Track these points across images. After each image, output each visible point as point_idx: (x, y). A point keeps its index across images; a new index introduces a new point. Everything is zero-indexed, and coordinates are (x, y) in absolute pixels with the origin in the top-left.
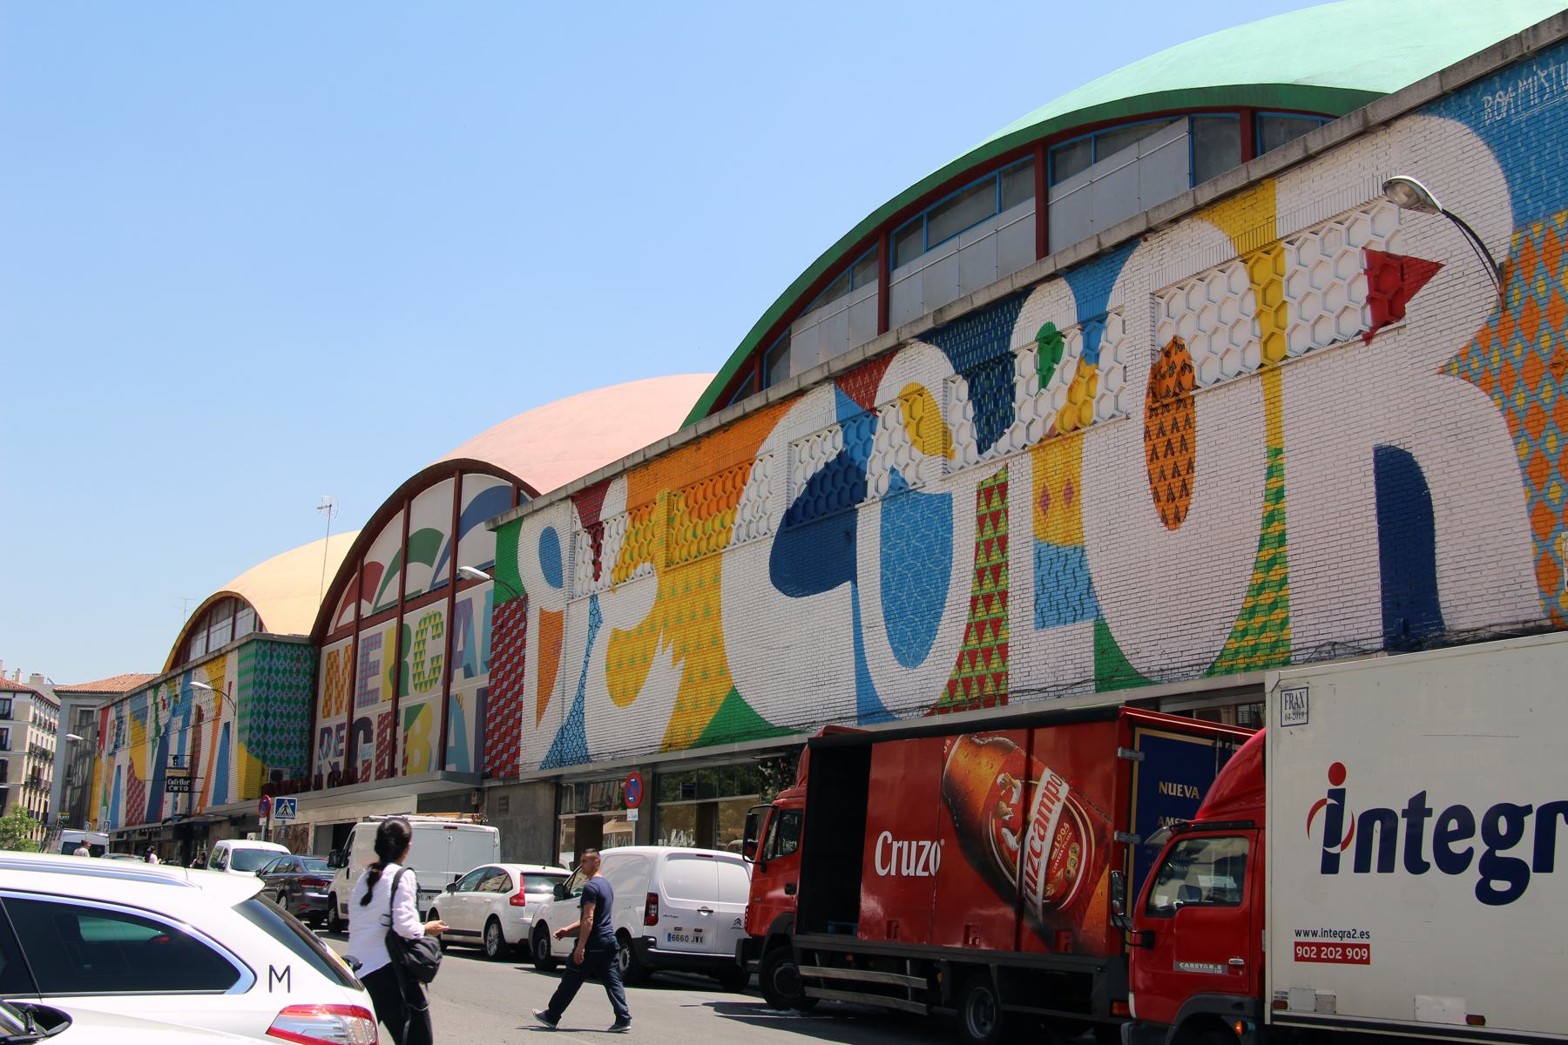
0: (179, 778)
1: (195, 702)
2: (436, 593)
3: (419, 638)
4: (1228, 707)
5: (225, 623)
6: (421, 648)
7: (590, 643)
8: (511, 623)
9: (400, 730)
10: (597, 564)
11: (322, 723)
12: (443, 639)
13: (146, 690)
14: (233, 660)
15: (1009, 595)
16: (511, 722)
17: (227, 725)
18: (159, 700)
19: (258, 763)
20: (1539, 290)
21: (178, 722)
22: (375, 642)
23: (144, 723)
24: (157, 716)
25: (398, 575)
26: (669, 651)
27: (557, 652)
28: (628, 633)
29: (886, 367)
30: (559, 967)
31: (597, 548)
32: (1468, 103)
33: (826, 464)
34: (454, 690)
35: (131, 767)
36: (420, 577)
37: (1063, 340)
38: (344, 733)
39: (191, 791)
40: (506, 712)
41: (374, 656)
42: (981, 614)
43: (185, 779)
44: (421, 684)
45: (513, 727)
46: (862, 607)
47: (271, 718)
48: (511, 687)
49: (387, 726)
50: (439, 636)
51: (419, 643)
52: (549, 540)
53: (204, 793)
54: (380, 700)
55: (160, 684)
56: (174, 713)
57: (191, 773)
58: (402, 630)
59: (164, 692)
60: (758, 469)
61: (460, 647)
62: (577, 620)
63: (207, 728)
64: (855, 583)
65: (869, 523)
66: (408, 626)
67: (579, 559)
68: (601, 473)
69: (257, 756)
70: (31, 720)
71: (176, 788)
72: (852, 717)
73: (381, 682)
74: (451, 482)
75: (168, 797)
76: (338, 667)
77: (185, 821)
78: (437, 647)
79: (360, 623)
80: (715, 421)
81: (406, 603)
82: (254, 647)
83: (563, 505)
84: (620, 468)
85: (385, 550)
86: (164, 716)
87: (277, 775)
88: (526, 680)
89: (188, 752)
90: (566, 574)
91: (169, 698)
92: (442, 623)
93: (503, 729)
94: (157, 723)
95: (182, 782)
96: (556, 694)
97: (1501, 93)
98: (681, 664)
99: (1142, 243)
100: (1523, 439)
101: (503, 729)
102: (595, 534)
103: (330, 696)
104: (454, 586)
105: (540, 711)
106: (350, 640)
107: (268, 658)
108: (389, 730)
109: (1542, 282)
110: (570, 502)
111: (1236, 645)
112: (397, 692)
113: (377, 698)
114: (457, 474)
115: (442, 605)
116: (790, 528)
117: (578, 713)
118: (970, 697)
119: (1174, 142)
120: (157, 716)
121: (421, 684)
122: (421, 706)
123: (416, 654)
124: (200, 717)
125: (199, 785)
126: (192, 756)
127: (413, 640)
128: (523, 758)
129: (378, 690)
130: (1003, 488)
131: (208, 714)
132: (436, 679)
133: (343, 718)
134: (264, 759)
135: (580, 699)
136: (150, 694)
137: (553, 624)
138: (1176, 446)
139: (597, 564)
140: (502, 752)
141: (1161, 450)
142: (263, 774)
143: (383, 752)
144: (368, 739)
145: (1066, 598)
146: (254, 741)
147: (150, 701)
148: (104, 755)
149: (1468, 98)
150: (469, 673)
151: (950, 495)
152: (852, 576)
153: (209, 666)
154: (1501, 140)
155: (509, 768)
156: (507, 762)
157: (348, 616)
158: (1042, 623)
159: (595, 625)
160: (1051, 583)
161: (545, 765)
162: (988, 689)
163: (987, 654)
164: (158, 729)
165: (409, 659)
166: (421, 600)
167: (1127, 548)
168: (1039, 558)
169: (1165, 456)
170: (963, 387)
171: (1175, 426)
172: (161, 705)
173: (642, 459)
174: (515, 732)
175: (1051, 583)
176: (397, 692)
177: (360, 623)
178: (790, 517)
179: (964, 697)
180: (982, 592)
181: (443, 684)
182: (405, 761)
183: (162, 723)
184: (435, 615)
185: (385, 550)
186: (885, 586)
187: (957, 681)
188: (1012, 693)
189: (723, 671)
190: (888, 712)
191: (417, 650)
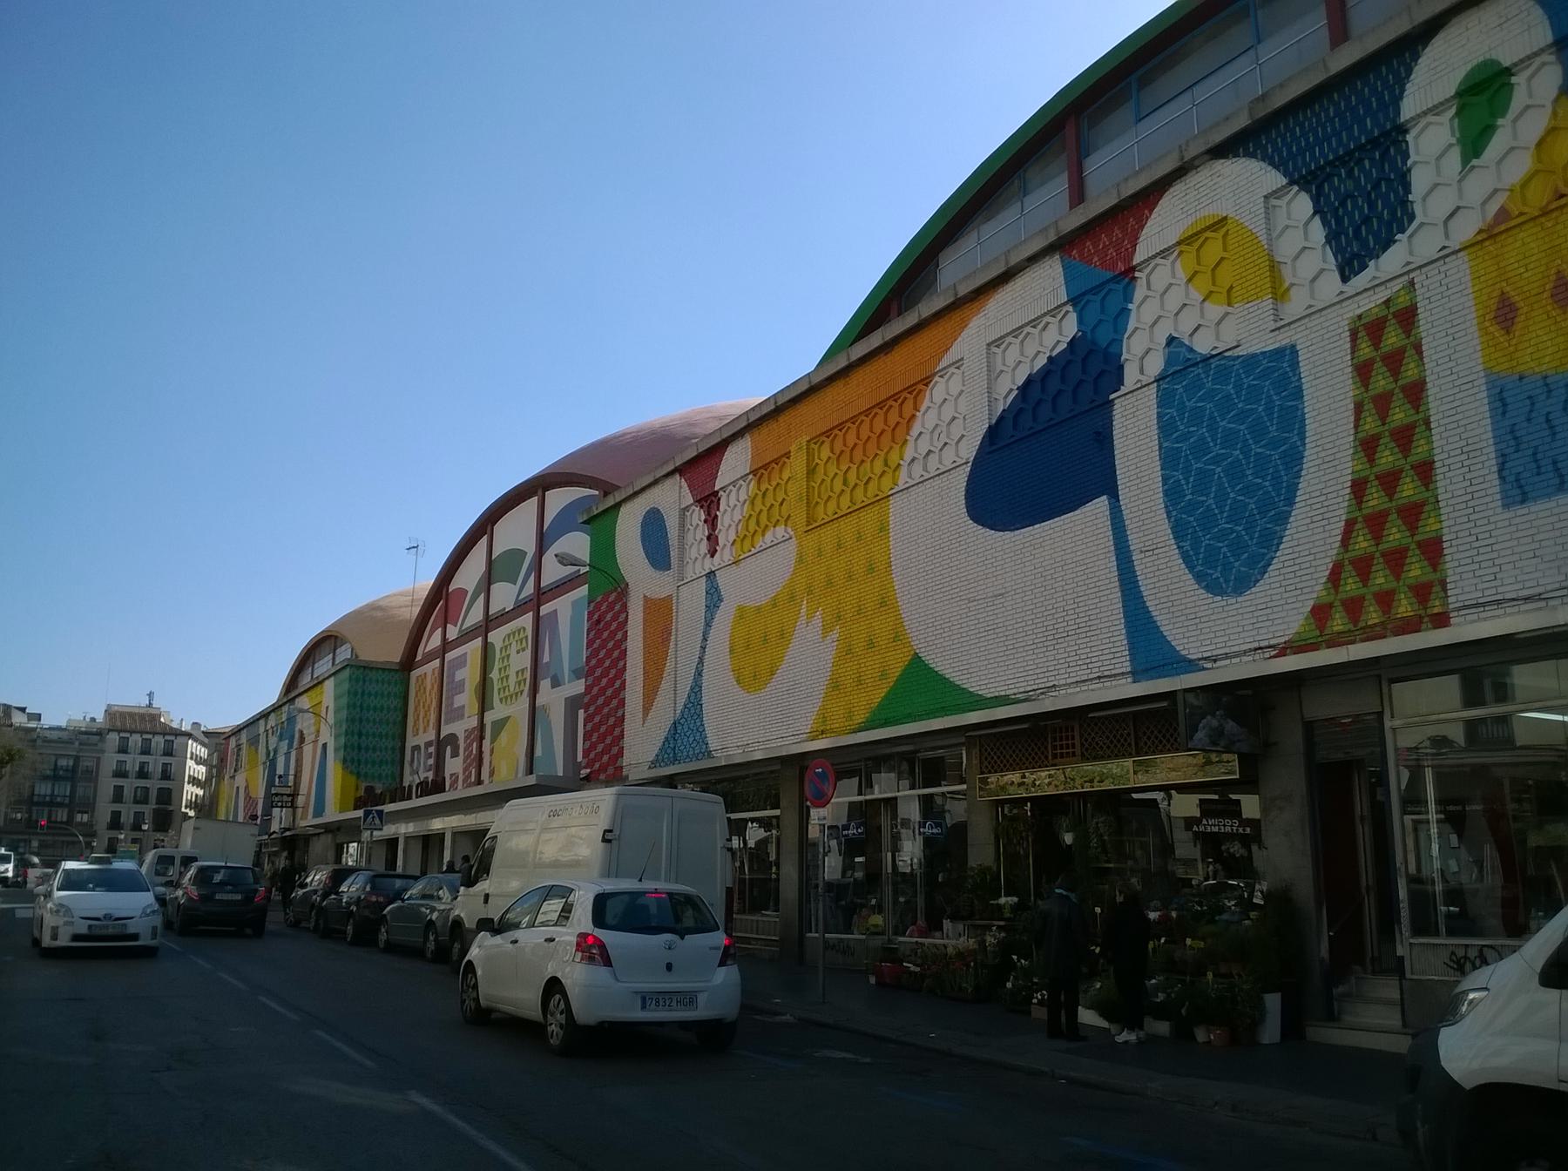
0: (282, 795)
1: (298, 727)
2: (520, 608)
3: (504, 654)
5: (326, 659)
6: (506, 663)
7: (708, 625)
8: (609, 617)
9: (486, 743)
10: (712, 539)
11: (411, 741)
12: (528, 652)
13: (258, 719)
14: (329, 685)
15: (1437, 465)
16: (612, 721)
17: (325, 746)
18: (269, 727)
19: (352, 779)
21: (284, 745)
22: (461, 662)
23: (257, 750)
24: (267, 741)
25: (482, 597)
26: (817, 621)
27: (666, 641)
28: (758, 609)
29: (1151, 211)
31: (712, 521)
33: (1050, 359)
34: (540, 701)
35: (247, 787)
36: (504, 596)
38: (432, 749)
39: (293, 806)
40: (606, 710)
41: (460, 675)
42: (1375, 499)
43: (288, 795)
44: (506, 698)
45: (614, 726)
46: (1131, 526)
47: (364, 738)
48: (611, 683)
49: (473, 741)
50: (523, 650)
51: (503, 658)
52: (653, 524)
53: (305, 807)
54: (466, 715)
55: (269, 713)
56: (281, 738)
57: (294, 790)
58: (487, 648)
59: (272, 721)
60: (938, 390)
61: (546, 658)
62: (692, 601)
63: (308, 749)
64: (1114, 495)
66: (493, 644)
67: (690, 537)
68: (718, 434)
69: (351, 772)
70: (189, 756)
71: (280, 804)
72: (1123, 674)
73: (466, 699)
74: (533, 502)
75: (276, 811)
76: (425, 689)
77: (288, 833)
78: (523, 660)
79: (446, 646)
80: (875, 340)
81: (490, 622)
82: (347, 672)
83: (669, 482)
84: (744, 424)
85: (470, 575)
86: (273, 740)
87: (369, 790)
88: (628, 675)
89: (292, 772)
90: (674, 554)
91: (277, 725)
92: (527, 637)
93: (603, 729)
94: (267, 748)
95: (285, 798)
96: (666, 686)
98: (835, 635)
101: (603, 729)
102: (709, 506)
103: (418, 715)
104: (539, 599)
105: (647, 709)
106: (437, 663)
107: (361, 683)
108: (475, 744)
110: (677, 476)
112: (484, 704)
113: (463, 715)
114: (540, 492)
115: (527, 620)
116: (994, 448)
117: (694, 704)
118: (1362, 624)
120: (267, 741)
121: (506, 698)
122: (509, 717)
123: (500, 669)
124: (302, 739)
125: (300, 800)
126: (295, 776)
127: (498, 656)
128: (626, 760)
129: (464, 706)
130: (1407, 317)
131: (309, 738)
132: (522, 692)
133: (431, 735)
134: (358, 775)
135: (696, 689)
136: (262, 722)
137: (660, 613)
139: (712, 539)
140: (602, 753)
142: (357, 789)
143: (470, 765)
144: (455, 754)
145: (1536, 461)
146: (349, 758)
147: (262, 729)
148: (226, 777)
150: (556, 683)
151: (1293, 346)
152: (1108, 485)
153: (309, 693)
155: (611, 770)
156: (608, 764)
157: (435, 641)
158: (1517, 491)
159: (714, 598)
161: (654, 764)
162: (1401, 610)
163: (1396, 560)
164: (268, 754)
165: (494, 675)
166: (505, 617)
167: (1085, 587)
168: (1502, 400)
170: (1303, 204)
172: (270, 732)
173: (773, 407)
174: (617, 731)
176: (484, 704)
177: (446, 646)
178: (993, 433)
179: (1351, 626)
180: (1375, 470)
181: (529, 695)
182: (492, 773)
183: (271, 748)
184: (519, 631)
185: (470, 575)
186: (1172, 494)
187: (1330, 606)
188: (1459, 609)
189: (898, 636)
190: (1191, 661)
191: (500, 686)
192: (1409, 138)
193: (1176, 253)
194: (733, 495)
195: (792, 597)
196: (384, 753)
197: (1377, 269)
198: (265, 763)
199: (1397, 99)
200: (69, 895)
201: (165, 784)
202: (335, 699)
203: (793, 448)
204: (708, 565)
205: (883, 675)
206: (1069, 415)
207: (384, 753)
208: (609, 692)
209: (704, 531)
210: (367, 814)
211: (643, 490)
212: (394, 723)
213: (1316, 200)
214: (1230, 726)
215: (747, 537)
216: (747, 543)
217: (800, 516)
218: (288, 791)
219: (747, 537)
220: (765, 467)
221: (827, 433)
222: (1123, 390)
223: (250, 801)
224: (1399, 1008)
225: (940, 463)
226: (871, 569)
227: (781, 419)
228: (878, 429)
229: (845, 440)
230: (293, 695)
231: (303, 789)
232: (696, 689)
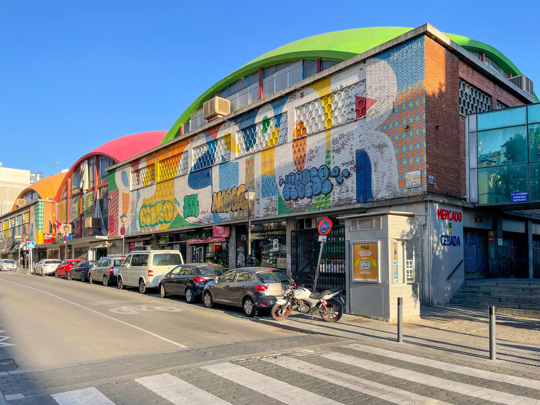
4: (314, 218)
6: (87, 204)
17: (32, 224)
20: (403, 108)
28: (148, 199)
32: (386, 55)
37: (270, 121)
44: (89, 213)
51: (87, 202)
58: (67, 203)
65: (215, 172)
97: (396, 52)
99: (190, 142)
100: (397, 148)
109: (404, 105)
111: (316, 202)
119: (298, 67)
132: (92, 212)
138: (301, 150)
141: (297, 151)
149: (386, 53)
154: (395, 66)
160: (266, 186)
169: (298, 152)
171: (301, 145)
175: (266, 186)
183: (13, 224)
193: (359, 84)
200: (248, 62)
201: (408, 274)
206: (345, 123)
224: (488, 340)
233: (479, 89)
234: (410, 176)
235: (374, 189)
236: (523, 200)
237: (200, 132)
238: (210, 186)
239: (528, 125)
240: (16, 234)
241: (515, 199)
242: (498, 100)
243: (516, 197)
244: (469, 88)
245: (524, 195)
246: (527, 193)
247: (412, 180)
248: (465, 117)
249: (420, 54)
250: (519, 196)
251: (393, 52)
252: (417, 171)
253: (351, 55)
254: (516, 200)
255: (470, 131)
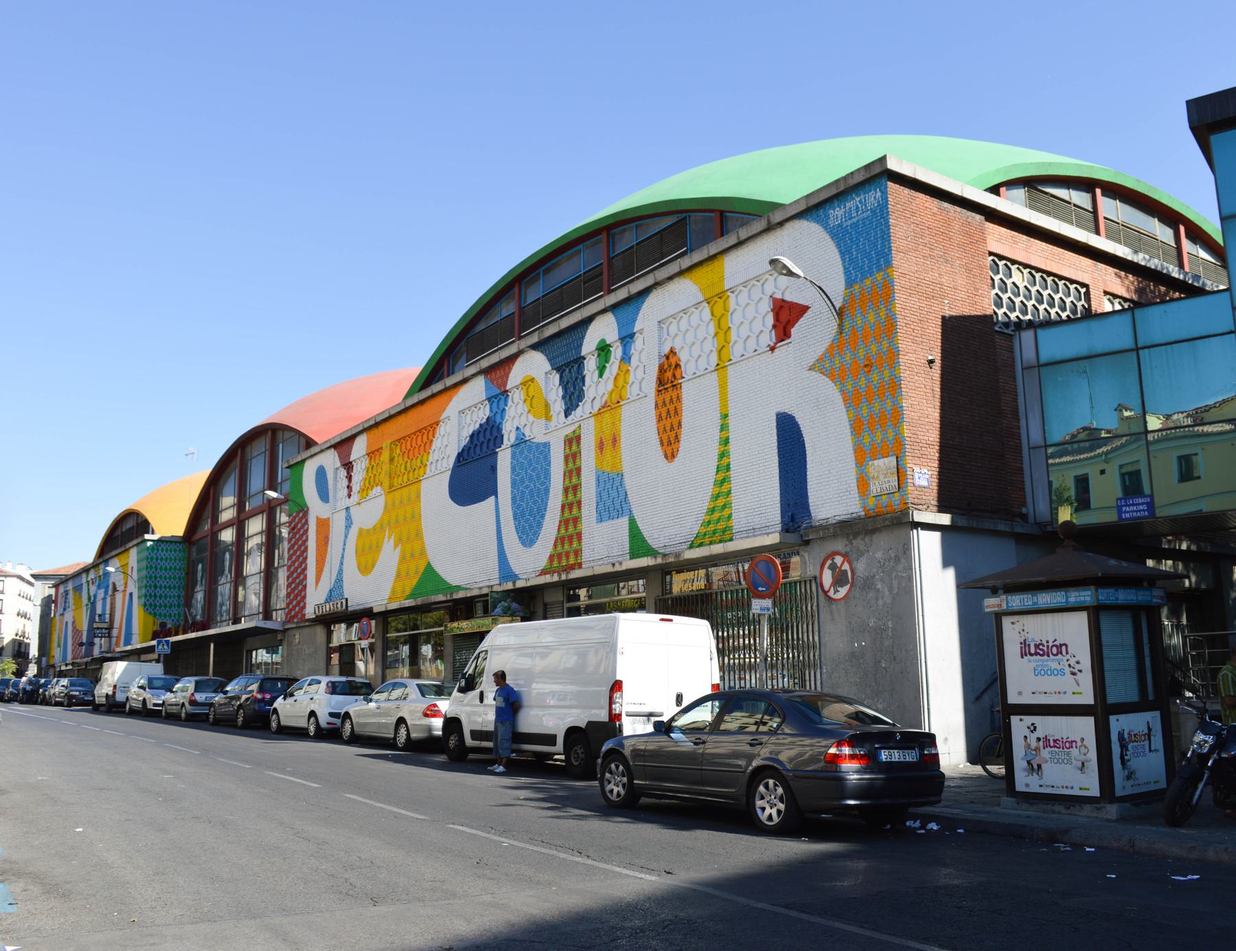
0: (102, 628)
10: (349, 487)
16: (300, 587)
17: (131, 594)
18: (89, 579)
19: (151, 619)
24: (89, 589)
26: (392, 541)
27: (327, 543)
28: (368, 531)
30: (1093, 850)
31: (349, 478)
39: (110, 636)
43: (106, 629)
53: (118, 637)
56: (99, 587)
59: (92, 575)
63: (119, 596)
64: (497, 497)
67: (339, 486)
69: (150, 613)
86: (93, 589)
87: (163, 625)
89: (108, 612)
90: (331, 494)
94: (89, 594)
95: (104, 631)
96: (326, 569)
117: (339, 580)
120: (89, 589)
125: (115, 632)
130: (578, 438)
134: (155, 615)
135: (340, 572)
136: (84, 575)
137: (324, 525)
138: (672, 412)
141: (664, 415)
146: (148, 603)
155: (300, 616)
158: (600, 519)
172: (90, 583)
174: (303, 593)
178: (460, 455)
183: (92, 594)
186: (514, 499)
187: (554, 556)
189: (423, 553)
192: (585, 362)
194: (419, 438)
195: (382, 527)
196: (172, 599)
197: (575, 416)
198: (87, 605)
199: (634, 320)
202: (138, 562)
203: (384, 446)
204: (349, 502)
205: (416, 572)
207: (172, 599)
208: (299, 571)
209: (345, 482)
210: (159, 643)
211: (315, 454)
212: (180, 578)
213: (561, 378)
214: (514, 605)
215: (365, 490)
216: (365, 493)
217: (386, 483)
218: (105, 626)
219: (365, 490)
220: (373, 453)
221: (399, 440)
222: (503, 447)
223: (77, 632)
225: (640, 390)
226: (413, 517)
227: (380, 428)
228: (694, 323)
229: (689, 321)
230: (107, 557)
231: (116, 624)
232: (340, 572)
233: (1050, 274)
234: (877, 470)
235: (812, 499)
236: (1142, 514)
237: (474, 376)
238: (493, 498)
239: (1137, 349)
240: (1122, 804)
241: (1126, 512)
242: (1106, 293)
243: (1128, 509)
244: (1022, 273)
245: (1143, 504)
246: (1149, 500)
247: (881, 477)
248: (1012, 335)
249: (882, 212)
250: (1133, 505)
251: (834, 210)
252: (890, 458)
253: (774, 206)
254: (1128, 515)
255: (1025, 365)
